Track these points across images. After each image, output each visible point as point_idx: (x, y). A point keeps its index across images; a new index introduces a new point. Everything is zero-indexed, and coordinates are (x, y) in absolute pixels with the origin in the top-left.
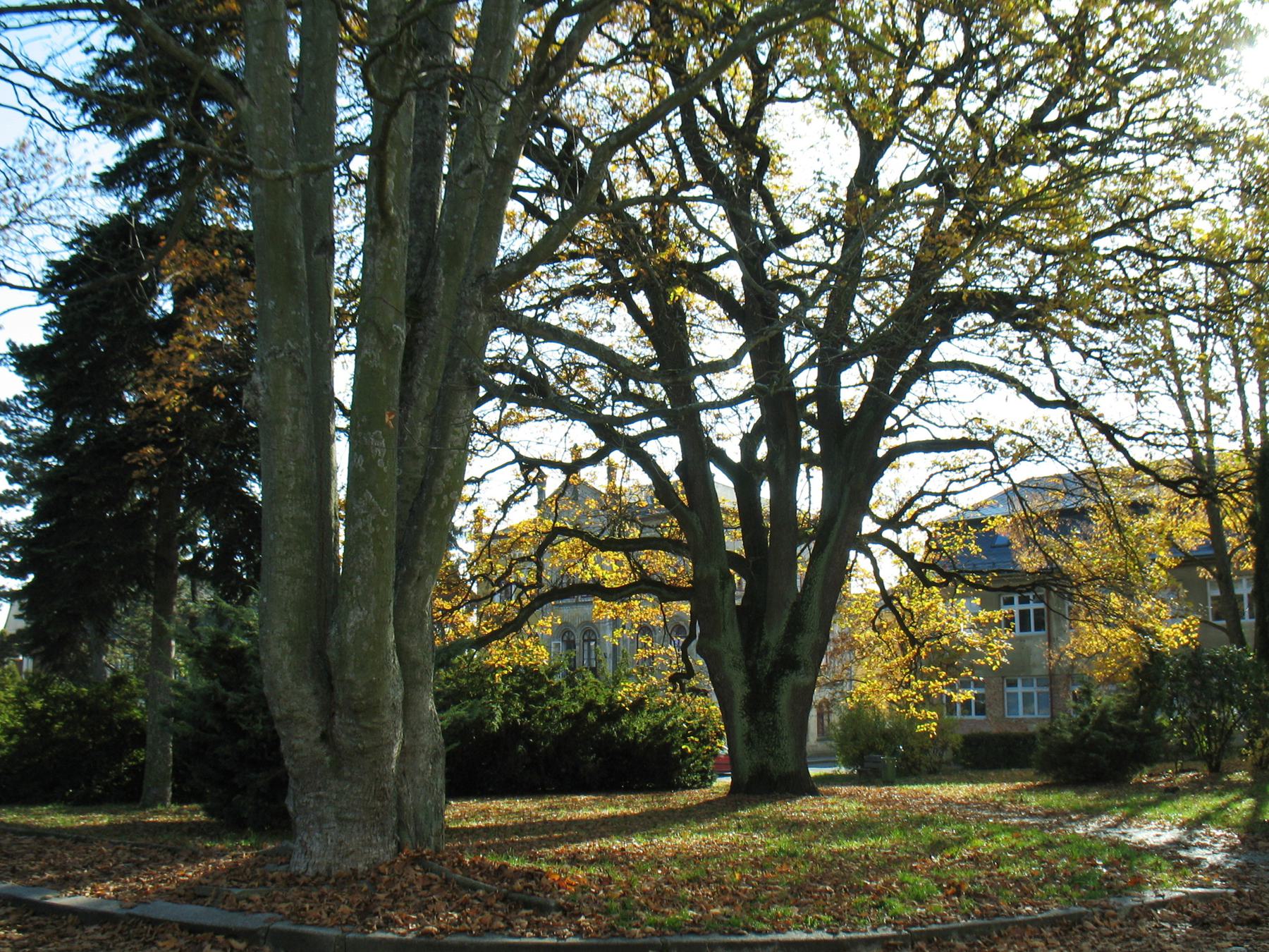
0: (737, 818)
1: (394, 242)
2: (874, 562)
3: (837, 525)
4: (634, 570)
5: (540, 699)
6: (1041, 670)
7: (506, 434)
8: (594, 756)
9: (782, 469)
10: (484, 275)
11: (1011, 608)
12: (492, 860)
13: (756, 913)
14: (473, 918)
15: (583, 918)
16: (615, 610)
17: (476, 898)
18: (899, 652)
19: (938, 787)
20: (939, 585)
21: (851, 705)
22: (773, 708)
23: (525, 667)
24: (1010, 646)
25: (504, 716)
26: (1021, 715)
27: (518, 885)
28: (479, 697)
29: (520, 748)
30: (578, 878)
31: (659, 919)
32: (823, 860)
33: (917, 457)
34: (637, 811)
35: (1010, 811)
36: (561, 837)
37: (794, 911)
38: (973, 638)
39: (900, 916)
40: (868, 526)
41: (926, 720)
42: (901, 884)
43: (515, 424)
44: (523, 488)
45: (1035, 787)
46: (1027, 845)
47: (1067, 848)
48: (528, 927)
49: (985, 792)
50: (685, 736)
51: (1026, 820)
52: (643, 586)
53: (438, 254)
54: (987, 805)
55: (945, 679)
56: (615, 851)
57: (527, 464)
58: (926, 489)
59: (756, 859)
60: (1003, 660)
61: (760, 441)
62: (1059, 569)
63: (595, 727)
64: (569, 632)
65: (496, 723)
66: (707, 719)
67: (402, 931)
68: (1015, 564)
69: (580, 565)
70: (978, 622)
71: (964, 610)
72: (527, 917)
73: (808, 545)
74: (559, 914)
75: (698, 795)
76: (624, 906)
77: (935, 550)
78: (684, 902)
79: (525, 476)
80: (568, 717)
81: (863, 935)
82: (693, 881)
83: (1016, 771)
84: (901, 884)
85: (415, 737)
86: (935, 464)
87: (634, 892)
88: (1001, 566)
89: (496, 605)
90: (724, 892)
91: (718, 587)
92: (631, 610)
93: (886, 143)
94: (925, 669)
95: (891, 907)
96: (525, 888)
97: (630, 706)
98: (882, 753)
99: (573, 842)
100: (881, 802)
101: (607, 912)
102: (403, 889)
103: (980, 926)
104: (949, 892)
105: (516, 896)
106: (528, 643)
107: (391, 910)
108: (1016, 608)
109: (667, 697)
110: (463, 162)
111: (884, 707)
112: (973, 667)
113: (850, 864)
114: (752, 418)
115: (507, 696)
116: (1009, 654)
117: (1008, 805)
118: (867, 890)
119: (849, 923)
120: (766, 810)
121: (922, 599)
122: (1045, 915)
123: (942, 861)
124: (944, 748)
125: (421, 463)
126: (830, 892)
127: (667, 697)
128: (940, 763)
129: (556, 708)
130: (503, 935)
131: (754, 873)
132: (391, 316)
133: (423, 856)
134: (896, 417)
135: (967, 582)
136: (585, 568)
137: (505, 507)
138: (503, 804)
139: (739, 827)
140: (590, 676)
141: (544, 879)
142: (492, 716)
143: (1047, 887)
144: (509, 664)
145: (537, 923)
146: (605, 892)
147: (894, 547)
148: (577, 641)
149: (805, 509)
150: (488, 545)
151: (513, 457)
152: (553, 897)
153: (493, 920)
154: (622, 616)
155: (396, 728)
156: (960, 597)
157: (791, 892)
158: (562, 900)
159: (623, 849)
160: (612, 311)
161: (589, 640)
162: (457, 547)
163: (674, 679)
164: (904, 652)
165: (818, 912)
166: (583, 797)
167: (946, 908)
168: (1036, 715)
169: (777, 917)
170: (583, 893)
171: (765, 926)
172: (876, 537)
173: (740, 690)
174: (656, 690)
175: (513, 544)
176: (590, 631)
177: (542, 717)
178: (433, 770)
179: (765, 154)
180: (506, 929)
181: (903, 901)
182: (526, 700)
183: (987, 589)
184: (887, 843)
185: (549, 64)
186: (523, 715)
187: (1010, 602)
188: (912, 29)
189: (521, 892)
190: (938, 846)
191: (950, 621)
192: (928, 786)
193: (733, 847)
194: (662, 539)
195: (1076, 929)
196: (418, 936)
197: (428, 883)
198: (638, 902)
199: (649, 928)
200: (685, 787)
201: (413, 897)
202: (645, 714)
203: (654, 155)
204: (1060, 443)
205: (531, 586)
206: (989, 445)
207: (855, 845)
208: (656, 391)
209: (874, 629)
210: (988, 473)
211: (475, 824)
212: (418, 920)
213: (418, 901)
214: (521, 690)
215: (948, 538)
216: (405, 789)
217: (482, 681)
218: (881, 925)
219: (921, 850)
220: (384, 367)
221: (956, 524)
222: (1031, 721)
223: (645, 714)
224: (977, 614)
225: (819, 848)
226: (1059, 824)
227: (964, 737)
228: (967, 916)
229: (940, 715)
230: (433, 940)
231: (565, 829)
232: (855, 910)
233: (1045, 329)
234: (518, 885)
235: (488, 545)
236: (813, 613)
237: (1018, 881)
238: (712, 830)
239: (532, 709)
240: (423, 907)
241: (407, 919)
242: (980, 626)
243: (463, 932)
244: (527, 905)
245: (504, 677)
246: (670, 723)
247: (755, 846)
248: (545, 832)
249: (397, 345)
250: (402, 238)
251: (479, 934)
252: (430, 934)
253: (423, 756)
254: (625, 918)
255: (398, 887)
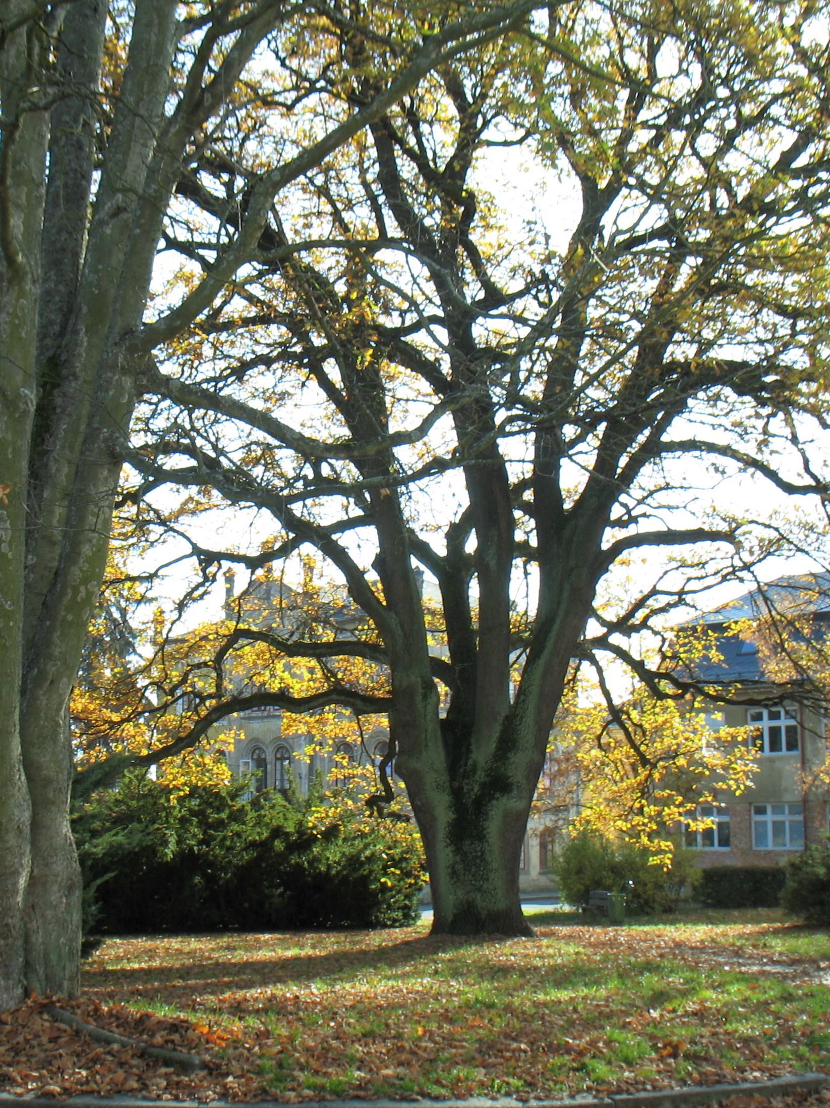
0: (435, 962)
1: (22, 294)
2: (600, 671)
3: (556, 627)
4: (327, 679)
5: (220, 825)
6: (794, 794)
7: (184, 523)
8: (281, 890)
9: (493, 564)
10: (129, 332)
11: (758, 725)
12: (134, 1009)
13: (434, 1076)
14: (103, 1076)
15: (230, 1079)
16: (306, 723)
17: (109, 1053)
18: (631, 774)
19: (672, 928)
20: (674, 697)
21: (574, 834)
22: (481, 837)
23: (205, 789)
24: (755, 768)
25: (179, 843)
26: (770, 846)
27: (158, 1039)
28: (153, 822)
29: (197, 879)
30: (231, 1032)
31: (319, 1080)
32: (524, 1013)
33: (646, 550)
34: (323, 953)
35: (751, 957)
36: (231, 982)
37: (480, 1074)
38: (712, 757)
39: (603, 1082)
40: (593, 629)
41: (660, 852)
42: (608, 1043)
43: (193, 513)
44: (202, 584)
45: (784, 929)
46: (763, 997)
47: (810, 1002)
48: (166, 1088)
49: (724, 935)
50: (385, 868)
51: (767, 968)
52: (334, 697)
53: (80, 309)
54: (724, 949)
55: (681, 805)
56: (287, 999)
57: (207, 558)
58: (658, 588)
59: (447, 1010)
60: (749, 783)
61: (470, 532)
62: (810, 680)
63: (283, 857)
64: (260, 749)
65: (170, 851)
66: (410, 850)
67: (19, 1090)
68: (763, 674)
69: (267, 673)
70: (718, 739)
71: (703, 726)
72: (167, 1076)
73: (525, 651)
74: (203, 1073)
75: (399, 934)
76: (280, 1065)
77: (671, 658)
78: (352, 1060)
79: (204, 571)
80: (253, 845)
81: (558, 1103)
82: (368, 1036)
83: (763, 911)
84: (608, 1043)
85: (47, 865)
86: (671, 559)
87: (295, 1049)
88: (746, 676)
89: (170, 718)
90: (401, 1049)
91: (419, 698)
92: (325, 724)
93: (612, 191)
94: (658, 793)
95: (594, 1070)
96: (167, 1042)
97: (322, 833)
98: (609, 889)
99: (241, 988)
100: (604, 944)
101: (260, 1072)
102: (27, 1041)
103: (698, 1094)
104: (665, 1052)
105: (155, 1051)
106: (207, 761)
107: (9, 1065)
108: (765, 724)
109: (365, 823)
110: (109, 205)
111: (611, 835)
112: (716, 793)
113: (554, 1018)
114: (460, 505)
115: (183, 821)
116: (755, 777)
117: (749, 950)
118: (568, 1050)
119: (543, 1089)
120: (471, 953)
121: (654, 714)
122: (776, 1082)
123: (662, 1016)
124: (682, 883)
125: (58, 550)
126: (525, 1051)
127: (365, 823)
128: (676, 901)
129: (238, 835)
130: (136, 1098)
131: (440, 1027)
132: (19, 378)
133: (53, 1003)
134: (625, 505)
135: (707, 695)
136: (273, 676)
137: (181, 607)
138: (175, 943)
139: (436, 972)
140: (279, 799)
141: (190, 1032)
142: (165, 843)
143: (780, 1048)
144: (185, 784)
145: (178, 1083)
146: (261, 1048)
147: (622, 654)
148: (269, 759)
149: (521, 609)
150: (162, 649)
151: (189, 549)
152: (198, 1053)
153: (126, 1080)
154: (314, 731)
155: (22, 855)
156: (699, 711)
157: (480, 1051)
158: (207, 1057)
159: (297, 997)
160: (303, 384)
161: (283, 759)
162: (134, 651)
163: (372, 802)
164: (636, 773)
165: (507, 1074)
166: (267, 936)
167: (659, 1072)
168: (788, 847)
169: (459, 1080)
170: (236, 1048)
171: (443, 1091)
172: (602, 642)
173: (444, 815)
174: (353, 815)
175: (190, 647)
176: (283, 747)
177: (222, 844)
178: (68, 904)
179: (470, 203)
180: (141, 1090)
181: (609, 1063)
182: (205, 824)
183: (729, 702)
184: (603, 992)
185: (203, 90)
186: (201, 843)
187: (758, 717)
188: (644, 64)
189: (162, 1047)
190: (659, 998)
191: (686, 739)
192: (661, 926)
193: (423, 997)
194: (358, 643)
195: (811, 1100)
196: (38, 1097)
197: (56, 1034)
198: (298, 1062)
199: (307, 1092)
200: (384, 926)
201: (36, 1050)
202: (340, 842)
203: (350, 206)
204: (813, 536)
205: (210, 696)
206: (729, 537)
207: (564, 995)
208: (348, 472)
209: (600, 746)
210: (731, 569)
211: (136, 966)
212: (40, 1078)
213: (42, 1055)
214: (200, 814)
215: (684, 645)
216: (34, 925)
217: (155, 803)
218: (579, 1091)
219: (639, 1002)
220: (9, 437)
221: (694, 629)
222: (781, 854)
223: (340, 842)
224: (717, 731)
225: (524, 999)
226: (805, 973)
227: (705, 871)
228: (683, 1082)
229: (677, 846)
230: (53, 1102)
231: (238, 973)
232: (550, 1073)
233: (794, 404)
234: (158, 1039)
235: (162, 649)
236: (526, 731)
237: (747, 1041)
238: (405, 976)
239: (212, 835)
240: (46, 1063)
241: (27, 1076)
242: (727, 746)
243: (91, 1092)
244: (167, 1063)
245: (181, 800)
246: (368, 853)
247: (451, 995)
248: (215, 976)
249: (25, 413)
250: (33, 289)
251: (108, 1096)
252: (51, 1095)
253: (55, 888)
254: (279, 1079)
255: (20, 1039)
